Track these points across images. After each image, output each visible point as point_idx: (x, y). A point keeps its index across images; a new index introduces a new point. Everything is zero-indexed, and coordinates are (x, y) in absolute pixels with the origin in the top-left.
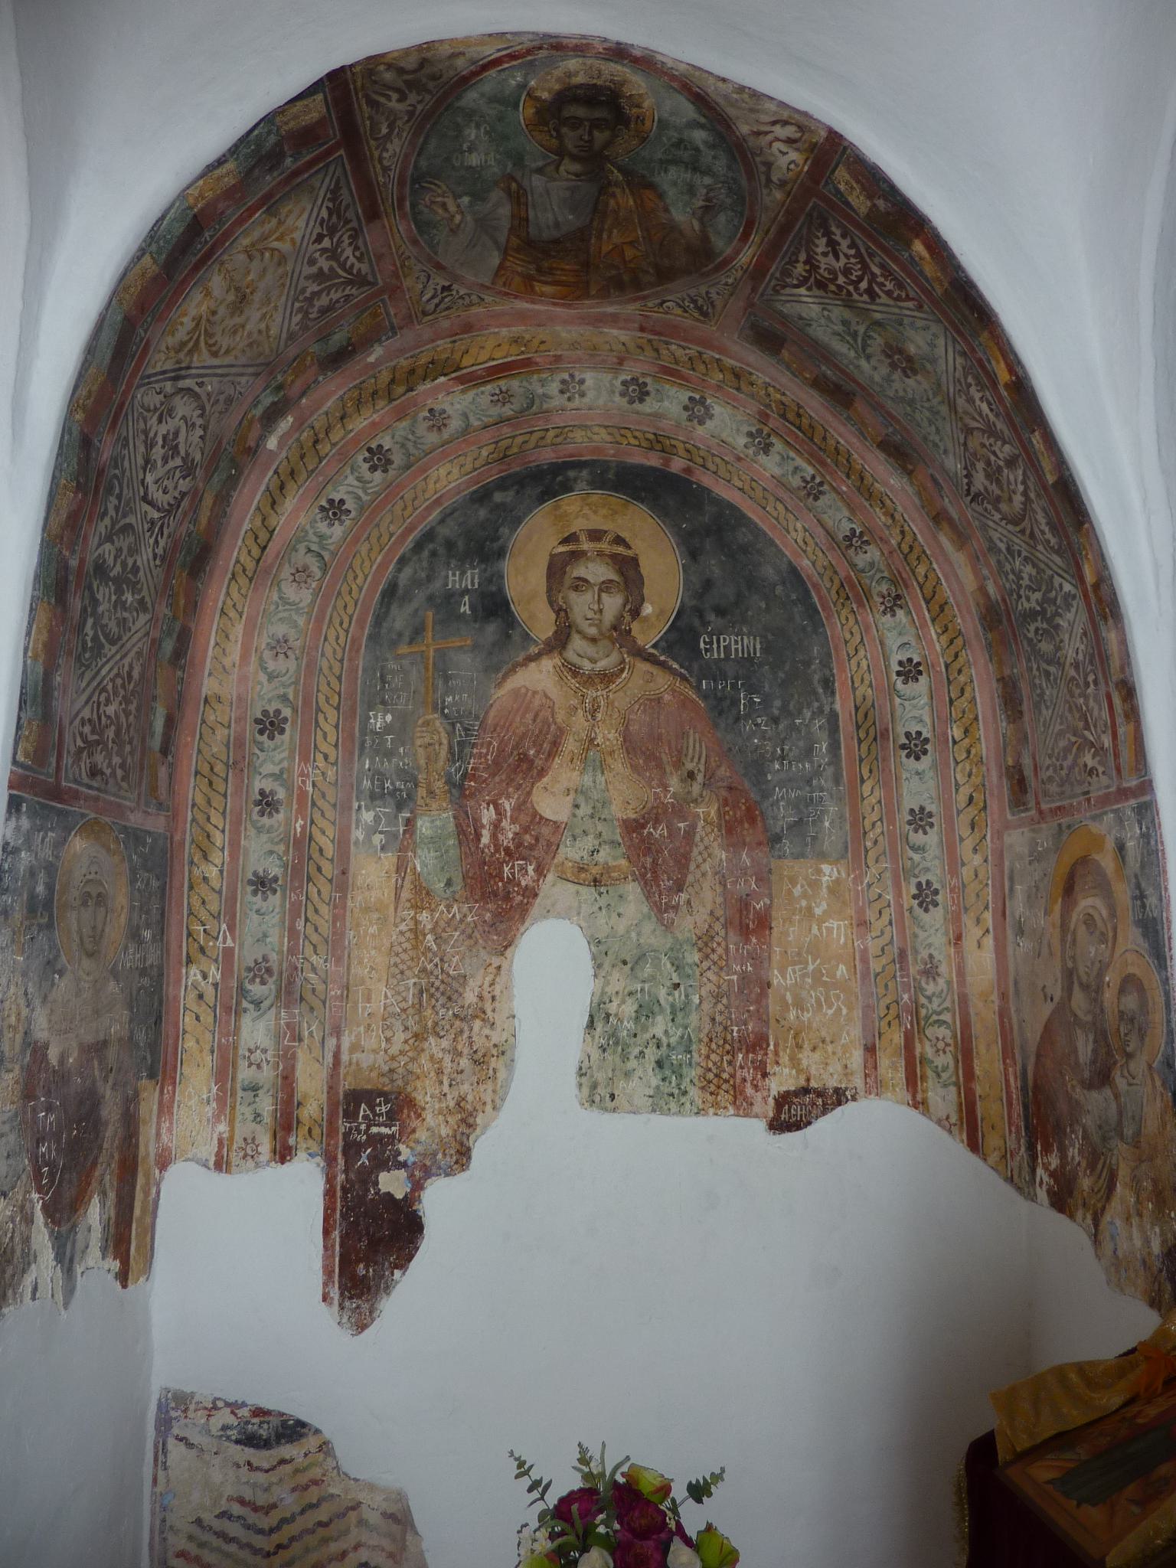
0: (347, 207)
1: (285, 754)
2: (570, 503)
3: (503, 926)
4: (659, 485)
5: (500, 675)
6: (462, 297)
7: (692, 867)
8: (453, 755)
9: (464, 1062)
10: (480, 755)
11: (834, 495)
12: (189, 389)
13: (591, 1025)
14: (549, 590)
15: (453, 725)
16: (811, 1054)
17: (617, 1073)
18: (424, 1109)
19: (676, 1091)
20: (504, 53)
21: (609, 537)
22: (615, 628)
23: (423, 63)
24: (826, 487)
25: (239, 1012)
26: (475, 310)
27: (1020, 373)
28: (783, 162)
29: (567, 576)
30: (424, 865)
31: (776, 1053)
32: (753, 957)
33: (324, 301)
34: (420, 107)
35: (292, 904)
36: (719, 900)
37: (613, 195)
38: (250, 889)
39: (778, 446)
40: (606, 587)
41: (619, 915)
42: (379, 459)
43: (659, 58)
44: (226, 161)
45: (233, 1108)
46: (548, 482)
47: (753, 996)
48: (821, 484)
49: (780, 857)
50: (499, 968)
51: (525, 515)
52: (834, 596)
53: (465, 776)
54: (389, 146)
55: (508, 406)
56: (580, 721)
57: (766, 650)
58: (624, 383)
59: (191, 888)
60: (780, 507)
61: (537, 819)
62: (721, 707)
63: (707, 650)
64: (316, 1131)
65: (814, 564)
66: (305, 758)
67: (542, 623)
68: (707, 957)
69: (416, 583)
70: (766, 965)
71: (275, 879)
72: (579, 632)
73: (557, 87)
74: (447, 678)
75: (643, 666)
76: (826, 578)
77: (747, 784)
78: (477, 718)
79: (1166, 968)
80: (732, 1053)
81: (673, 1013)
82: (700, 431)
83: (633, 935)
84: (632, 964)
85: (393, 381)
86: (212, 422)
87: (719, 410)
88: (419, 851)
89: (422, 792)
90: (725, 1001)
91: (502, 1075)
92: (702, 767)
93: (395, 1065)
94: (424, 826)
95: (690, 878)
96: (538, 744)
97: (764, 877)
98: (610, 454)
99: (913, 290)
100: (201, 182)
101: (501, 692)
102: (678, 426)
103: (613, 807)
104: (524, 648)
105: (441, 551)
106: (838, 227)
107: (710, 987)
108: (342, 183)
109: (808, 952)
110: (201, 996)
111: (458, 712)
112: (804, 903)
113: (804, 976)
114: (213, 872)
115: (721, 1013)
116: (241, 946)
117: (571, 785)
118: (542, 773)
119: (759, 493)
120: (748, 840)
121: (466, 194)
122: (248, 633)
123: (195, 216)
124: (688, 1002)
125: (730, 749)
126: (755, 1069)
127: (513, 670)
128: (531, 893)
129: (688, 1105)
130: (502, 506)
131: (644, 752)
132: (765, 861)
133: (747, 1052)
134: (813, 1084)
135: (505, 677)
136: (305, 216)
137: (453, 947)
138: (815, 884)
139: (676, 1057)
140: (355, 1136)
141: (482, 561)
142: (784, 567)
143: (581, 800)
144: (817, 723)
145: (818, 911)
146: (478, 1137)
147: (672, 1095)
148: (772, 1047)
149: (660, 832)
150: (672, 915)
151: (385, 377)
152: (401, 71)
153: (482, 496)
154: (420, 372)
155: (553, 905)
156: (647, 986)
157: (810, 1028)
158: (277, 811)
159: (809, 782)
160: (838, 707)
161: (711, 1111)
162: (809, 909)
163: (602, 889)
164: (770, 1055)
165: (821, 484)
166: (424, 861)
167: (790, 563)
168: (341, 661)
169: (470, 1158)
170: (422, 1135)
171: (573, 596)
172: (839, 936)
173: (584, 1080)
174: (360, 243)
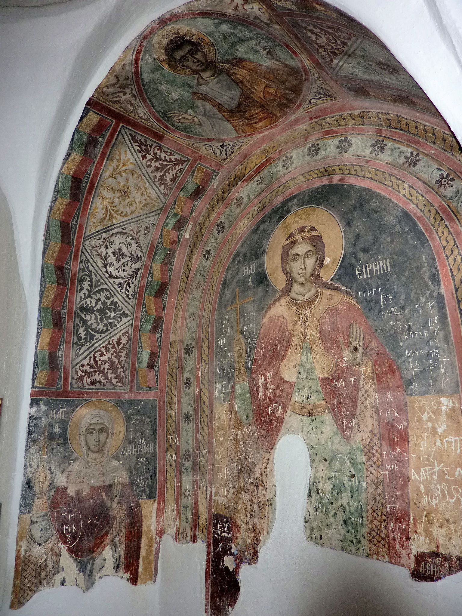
0: (145, 141)
1: (193, 362)
2: (290, 219)
3: (269, 438)
4: (329, 194)
5: (264, 312)
6: (233, 146)
7: (359, 403)
8: (247, 354)
9: (255, 507)
10: (258, 352)
11: (426, 158)
12: (118, 232)
13: (310, 494)
14: (283, 264)
15: (247, 339)
16: (439, 529)
17: (323, 523)
18: (240, 528)
19: (355, 540)
20: (135, 53)
21: (308, 229)
22: (312, 275)
24: (421, 156)
25: (182, 473)
26: (244, 148)
29: (290, 255)
30: (238, 407)
31: (415, 525)
32: (399, 461)
33: (169, 176)
34: (134, 92)
35: (196, 426)
36: (376, 423)
37: (235, 74)
38: (184, 420)
39: (389, 144)
40: (307, 255)
41: (322, 432)
42: (220, 227)
43: (175, 11)
44: (70, 154)
45: (180, 515)
46: (280, 213)
47: (399, 486)
48: (417, 155)
49: (412, 395)
50: (268, 460)
51: (272, 231)
52: (433, 221)
53: (252, 363)
54: (139, 112)
55: (264, 183)
56: (299, 328)
57: (393, 266)
58: (309, 149)
59: (167, 420)
60: (393, 179)
61: (283, 381)
62: (371, 306)
63: (360, 275)
64: (204, 531)
65: (417, 206)
66: (199, 363)
67: (278, 280)
68: (370, 459)
69: (233, 277)
70: (406, 466)
71: (191, 416)
72: (296, 282)
73: (162, 51)
74: (244, 317)
75: (327, 292)
76: (426, 212)
77: (388, 351)
78: (256, 334)
80: (386, 521)
81: (352, 492)
82: (346, 156)
83: (329, 444)
84: (329, 461)
85: (223, 192)
86: (141, 240)
87: (354, 140)
88: (236, 401)
89: (237, 373)
90: (381, 487)
91: (271, 516)
92: (361, 344)
93: (230, 504)
94: (238, 389)
95: (358, 410)
96: (281, 343)
97: (402, 408)
98: (305, 187)
100: (66, 165)
101: (265, 320)
102: (335, 158)
103: (317, 372)
104: (274, 296)
105: (242, 259)
107: (372, 477)
108: (134, 134)
109: (434, 458)
110: (171, 465)
111: (249, 333)
112: (430, 425)
113: (432, 474)
114: (173, 413)
115: (379, 495)
116: (181, 444)
117: (297, 362)
118: (284, 357)
119: (380, 175)
120: (391, 385)
121: (188, 109)
122: (183, 314)
123: (72, 177)
124: (360, 486)
125: (376, 330)
126: (401, 533)
127: (269, 308)
128: (281, 421)
129: (361, 550)
130: (264, 231)
131: (331, 340)
132: (402, 398)
133: (396, 522)
134: (442, 551)
135: (266, 313)
136: (128, 152)
137: (250, 448)
138: (437, 412)
139: (355, 519)
140: (216, 536)
141: (256, 259)
142: (399, 213)
143: (301, 370)
144: (430, 304)
145: (440, 430)
146: (261, 547)
147: (352, 542)
148: (412, 521)
149: (341, 384)
150: (349, 433)
151: (221, 191)
152: (113, 85)
153: (256, 229)
154: (232, 184)
155: (290, 427)
156: (337, 474)
157: (437, 511)
158: (191, 386)
159: (428, 344)
160: (443, 291)
161: (375, 556)
162: (434, 429)
163: (313, 418)
164: (411, 526)
165: (417, 155)
166: (238, 405)
167: (402, 210)
168: (209, 319)
169: (258, 557)
170: (240, 541)
171: (292, 264)
172: (456, 447)
173: (307, 525)
174: (165, 149)
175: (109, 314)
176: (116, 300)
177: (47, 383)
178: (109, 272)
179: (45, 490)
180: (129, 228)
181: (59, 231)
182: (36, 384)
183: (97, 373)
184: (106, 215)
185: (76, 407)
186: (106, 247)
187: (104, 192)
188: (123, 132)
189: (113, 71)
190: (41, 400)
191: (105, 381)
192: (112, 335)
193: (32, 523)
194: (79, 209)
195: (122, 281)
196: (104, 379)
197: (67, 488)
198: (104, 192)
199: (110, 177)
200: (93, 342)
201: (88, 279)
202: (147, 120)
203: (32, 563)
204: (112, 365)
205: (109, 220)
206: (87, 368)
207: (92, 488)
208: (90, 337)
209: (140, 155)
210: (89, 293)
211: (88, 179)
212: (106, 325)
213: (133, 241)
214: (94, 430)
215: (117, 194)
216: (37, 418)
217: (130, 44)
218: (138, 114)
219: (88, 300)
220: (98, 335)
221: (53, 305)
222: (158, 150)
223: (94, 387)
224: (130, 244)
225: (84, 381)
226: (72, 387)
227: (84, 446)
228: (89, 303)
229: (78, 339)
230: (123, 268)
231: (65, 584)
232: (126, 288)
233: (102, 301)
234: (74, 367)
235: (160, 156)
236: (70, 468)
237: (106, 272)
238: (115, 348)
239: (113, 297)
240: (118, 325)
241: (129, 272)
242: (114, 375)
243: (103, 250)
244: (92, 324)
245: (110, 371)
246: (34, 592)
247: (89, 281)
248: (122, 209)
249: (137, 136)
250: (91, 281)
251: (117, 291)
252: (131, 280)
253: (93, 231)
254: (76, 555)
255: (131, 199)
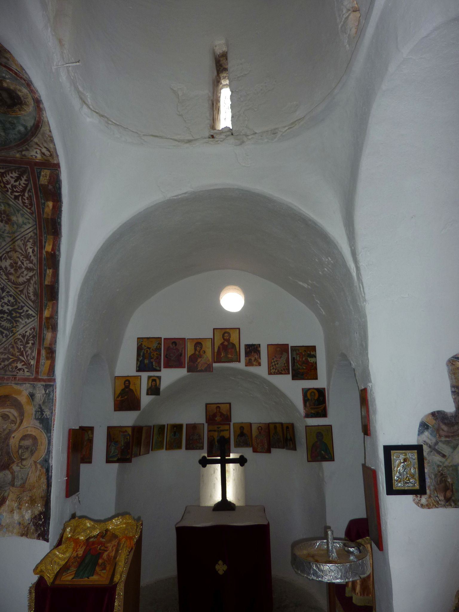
27: (57, 253)
28: (33, 153)
43: (44, 112)
79: (50, 433)
99: (35, 208)
106: (27, 177)
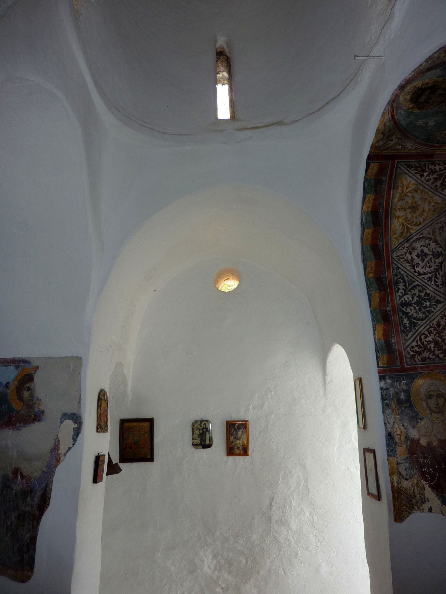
0: (419, 164)
23: (383, 133)
34: (399, 136)
86: (438, 238)
100: (364, 206)
108: (408, 163)
136: (408, 178)
152: (381, 139)
174: (437, 162)
175: (425, 303)
176: (428, 291)
177: (388, 363)
178: (417, 271)
179: (403, 441)
180: (425, 232)
181: (371, 252)
182: (380, 365)
183: (425, 352)
184: (404, 230)
185: (414, 379)
186: (410, 253)
187: (398, 213)
188: (400, 166)
189: (379, 131)
190: (386, 375)
191: (434, 357)
192: (431, 319)
193: (398, 464)
194: (382, 232)
195: (430, 275)
196: (432, 356)
197: (419, 440)
198: (398, 213)
199: (399, 200)
200: (417, 328)
201: (402, 281)
202: (415, 149)
203: (404, 492)
204: (436, 343)
205: (407, 232)
206: (416, 348)
207: (440, 441)
208: (413, 325)
209: (418, 175)
210: (405, 292)
211: (383, 209)
212: (424, 313)
213: (431, 241)
214: (433, 396)
215: (408, 211)
216: (386, 389)
217: (385, 110)
218: (407, 148)
219: (405, 297)
220: (419, 322)
221: (380, 306)
222: (432, 165)
223: (425, 362)
224: (429, 244)
225: (416, 359)
226: (407, 365)
227: (426, 408)
228: (406, 299)
229: (404, 328)
230: (428, 265)
231: (433, 511)
232: (435, 280)
233: (417, 295)
234: (406, 349)
235: (435, 169)
236: (419, 425)
237: (415, 272)
238: (436, 330)
239: (425, 290)
240: (435, 311)
241: (434, 267)
242: (440, 352)
243: (408, 256)
244: (413, 314)
245: (436, 349)
246: (410, 513)
247: (403, 283)
248: (415, 220)
249: (411, 163)
250: (404, 282)
251: (428, 285)
252: (437, 273)
253: (397, 244)
254: (437, 491)
255: (421, 210)
